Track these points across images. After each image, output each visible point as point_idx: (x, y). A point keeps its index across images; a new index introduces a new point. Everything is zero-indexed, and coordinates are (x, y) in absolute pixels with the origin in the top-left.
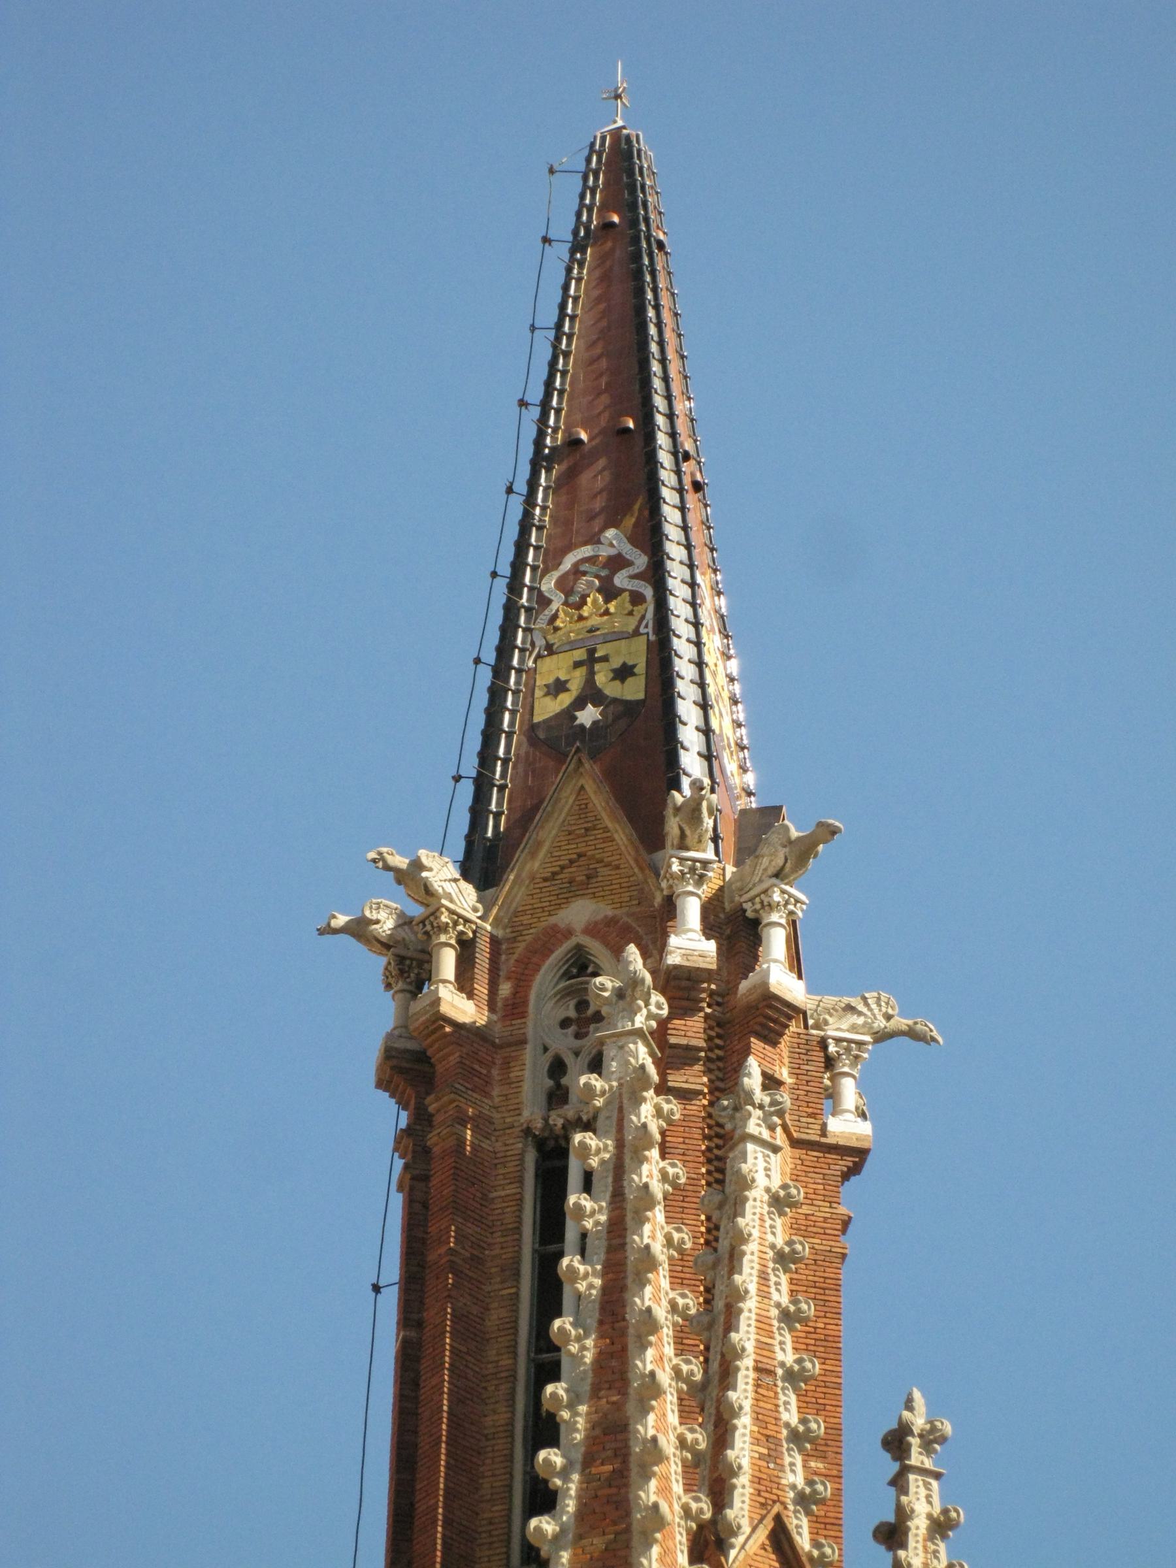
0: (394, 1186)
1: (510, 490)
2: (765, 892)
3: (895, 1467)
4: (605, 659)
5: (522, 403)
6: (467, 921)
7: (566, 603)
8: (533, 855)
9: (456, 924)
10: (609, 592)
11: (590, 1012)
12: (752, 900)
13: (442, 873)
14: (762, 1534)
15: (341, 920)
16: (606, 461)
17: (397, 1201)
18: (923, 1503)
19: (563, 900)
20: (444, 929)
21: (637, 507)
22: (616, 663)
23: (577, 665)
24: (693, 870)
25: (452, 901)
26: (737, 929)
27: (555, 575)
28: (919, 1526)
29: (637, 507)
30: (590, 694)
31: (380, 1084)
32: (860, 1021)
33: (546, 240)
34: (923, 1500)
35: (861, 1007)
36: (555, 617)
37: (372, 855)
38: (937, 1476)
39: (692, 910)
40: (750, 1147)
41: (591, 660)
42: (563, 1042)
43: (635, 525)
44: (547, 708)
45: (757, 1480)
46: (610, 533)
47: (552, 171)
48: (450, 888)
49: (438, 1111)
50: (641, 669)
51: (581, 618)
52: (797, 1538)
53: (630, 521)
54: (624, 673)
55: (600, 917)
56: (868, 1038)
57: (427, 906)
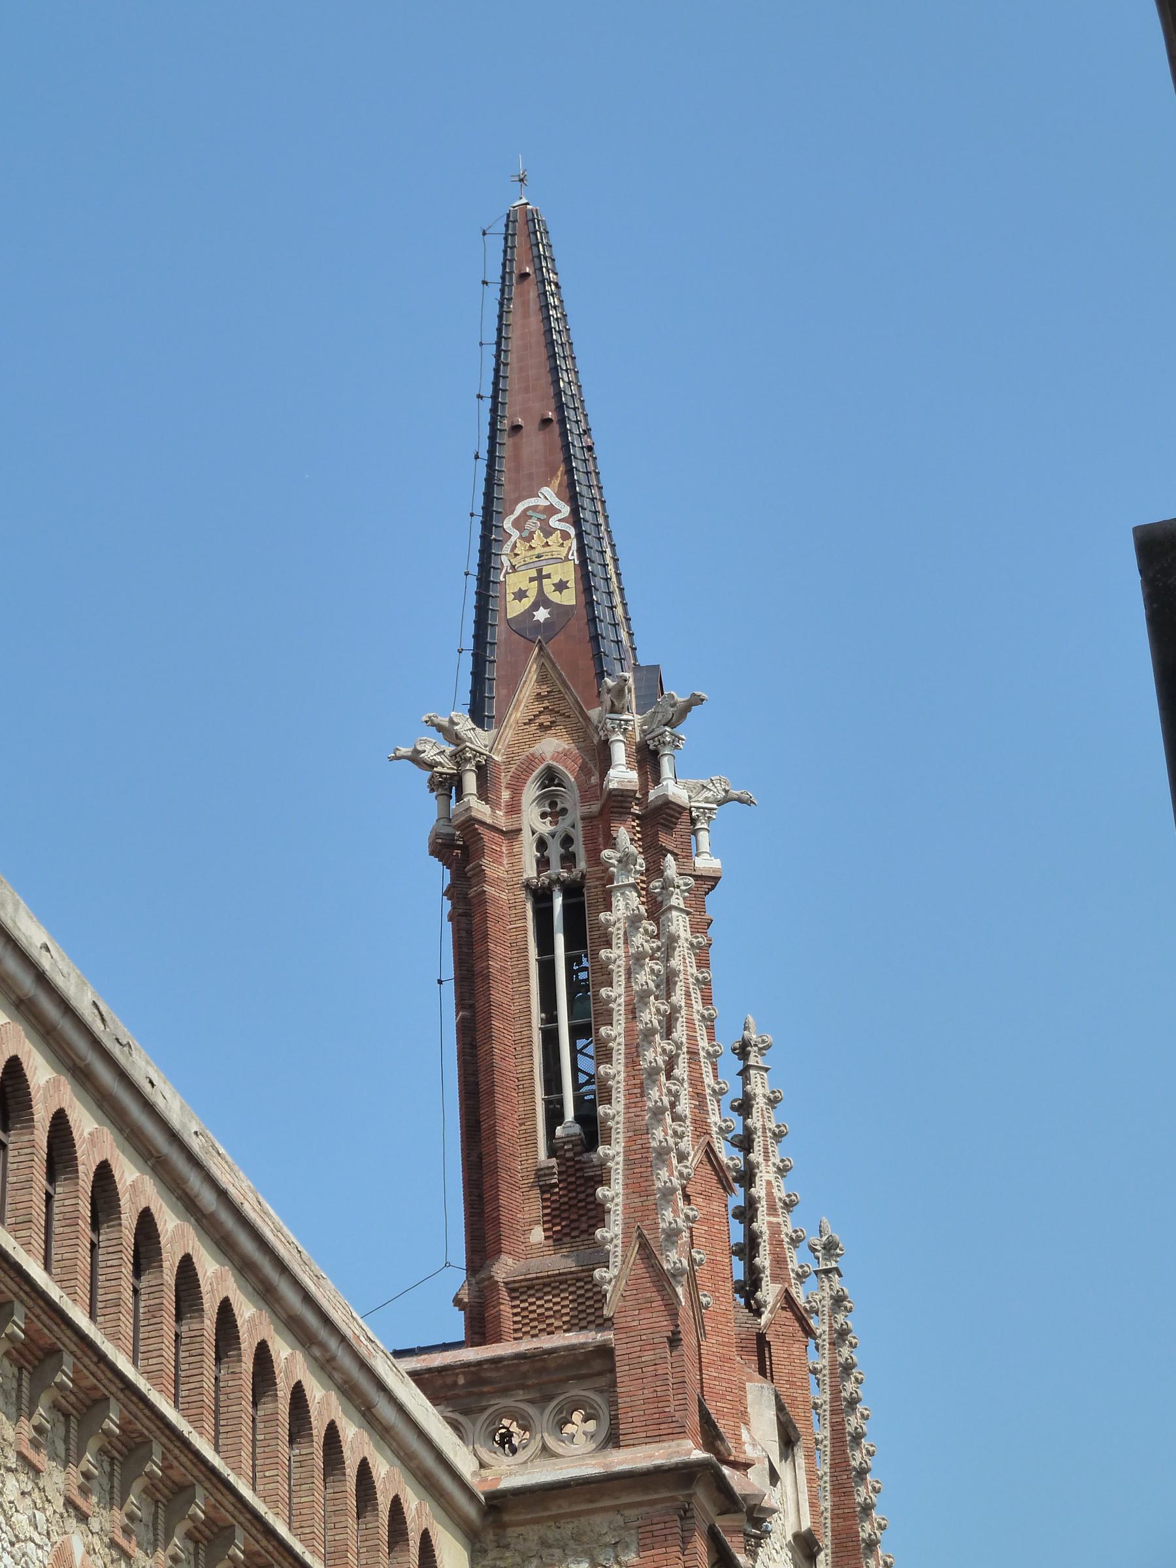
0: (445, 918)
1: (477, 457)
2: (661, 734)
3: (740, 1065)
4: (548, 576)
5: (480, 397)
6: (482, 754)
7: (521, 537)
8: (516, 708)
9: (475, 756)
10: (548, 531)
11: (558, 809)
12: (653, 739)
13: (465, 725)
14: (700, 1155)
15: (405, 750)
16: (536, 429)
17: (448, 926)
18: (759, 1087)
19: (536, 739)
20: (468, 760)
21: (559, 473)
22: (556, 579)
23: (531, 580)
24: (620, 725)
25: (472, 743)
26: (648, 759)
27: (512, 517)
28: (760, 1103)
29: (559, 473)
30: (542, 601)
31: (431, 854)
32: (710, 794)
33: (485, 283)
34: (760, 1085)
35: (710, 786)
36: (514, 546)
37: (425, 718)
38: (766, 1070)
39: (619, 752)
40: (674, 913)
41: (540, 577)
42: (545, 828)
43: (560, 485)
44: (515, 609)
45: (694, 1121)
46: (546, 490)
47: (484, 234)
48: (470, 734)
49: (474, 875)
50: (571, 584)
51: (531, 548)
52: (719, 1155)
53: (556, 482)
54: (561, 586)
55: (560, 750)
56: (714, 806)
57: (458, 745)
